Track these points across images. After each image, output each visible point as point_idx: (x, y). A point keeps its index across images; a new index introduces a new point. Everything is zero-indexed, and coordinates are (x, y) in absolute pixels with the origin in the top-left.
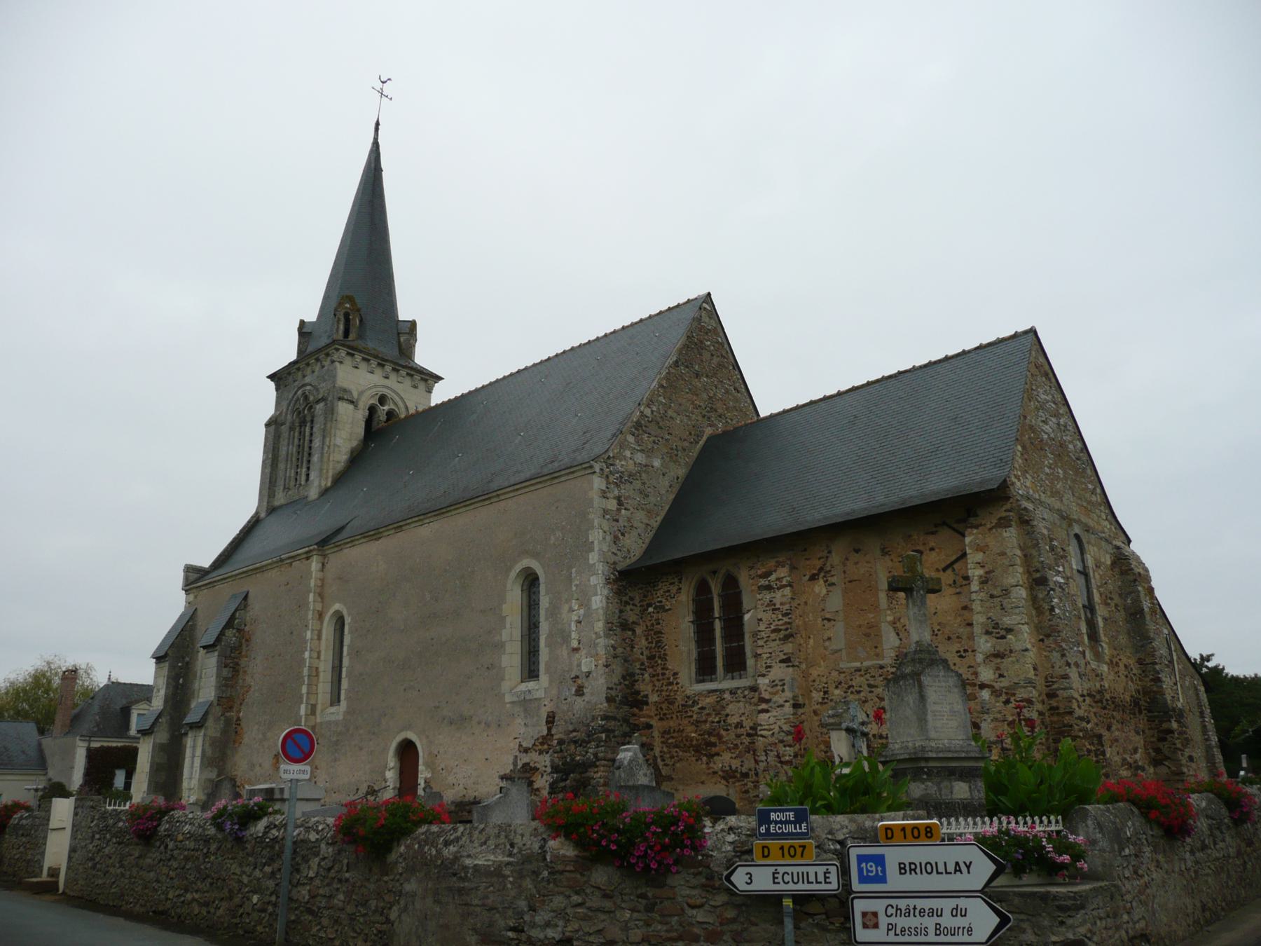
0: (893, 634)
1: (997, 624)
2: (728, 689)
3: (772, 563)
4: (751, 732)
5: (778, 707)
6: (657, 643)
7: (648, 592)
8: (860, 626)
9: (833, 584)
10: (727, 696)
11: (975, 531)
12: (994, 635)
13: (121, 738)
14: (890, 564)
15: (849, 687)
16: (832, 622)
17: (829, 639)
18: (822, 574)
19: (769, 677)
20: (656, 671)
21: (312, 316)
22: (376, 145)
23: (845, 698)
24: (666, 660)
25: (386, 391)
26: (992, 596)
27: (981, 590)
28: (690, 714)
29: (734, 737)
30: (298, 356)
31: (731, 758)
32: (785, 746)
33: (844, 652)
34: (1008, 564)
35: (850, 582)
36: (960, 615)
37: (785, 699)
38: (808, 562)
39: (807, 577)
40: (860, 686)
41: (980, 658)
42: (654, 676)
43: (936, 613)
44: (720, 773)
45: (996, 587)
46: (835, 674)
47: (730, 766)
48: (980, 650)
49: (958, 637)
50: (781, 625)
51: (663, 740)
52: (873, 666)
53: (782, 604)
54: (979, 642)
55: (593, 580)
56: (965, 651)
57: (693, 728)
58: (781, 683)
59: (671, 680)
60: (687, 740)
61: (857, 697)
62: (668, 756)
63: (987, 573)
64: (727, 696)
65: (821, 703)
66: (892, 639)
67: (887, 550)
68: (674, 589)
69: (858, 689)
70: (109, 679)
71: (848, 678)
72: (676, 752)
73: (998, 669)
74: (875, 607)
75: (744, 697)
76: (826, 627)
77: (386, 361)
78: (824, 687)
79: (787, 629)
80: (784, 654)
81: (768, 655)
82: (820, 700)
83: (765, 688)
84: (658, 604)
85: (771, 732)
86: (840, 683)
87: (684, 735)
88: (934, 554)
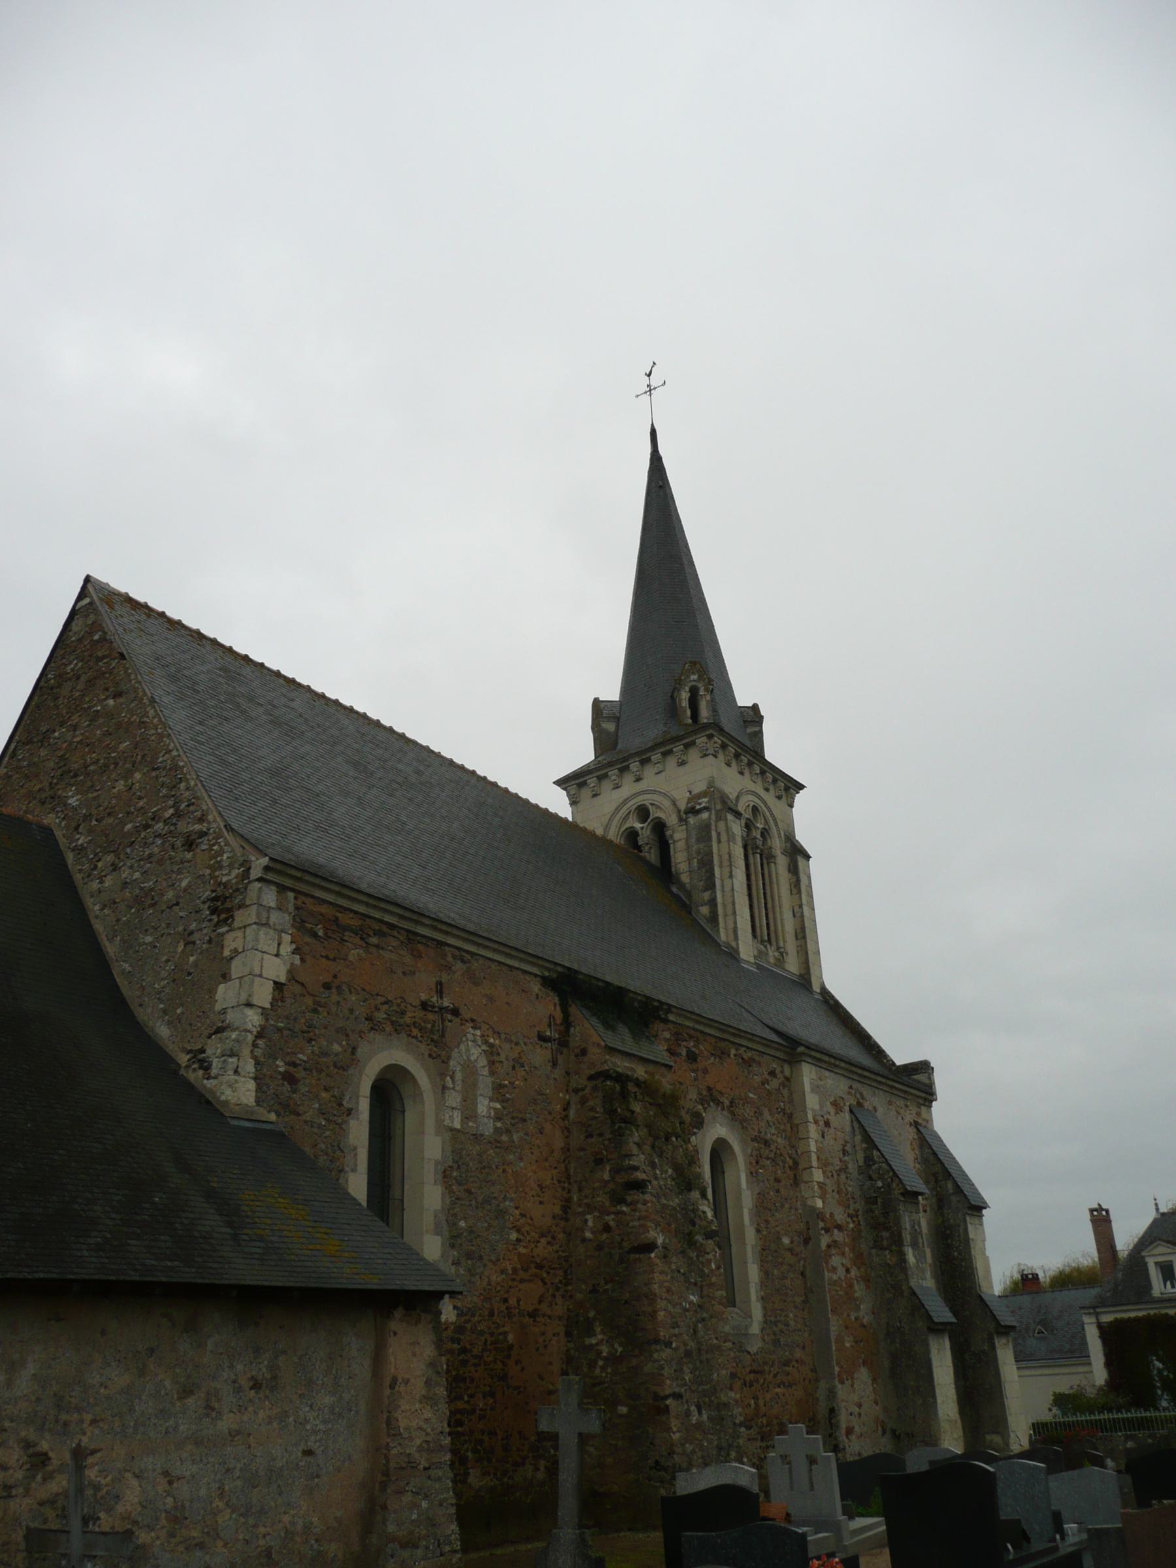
13: (1137, 1303)
21: (612, 692)
22: (656, 463)
25: (639, 800)
30: (597, 754)
70: (1157, 1209)
77: (625, 759)
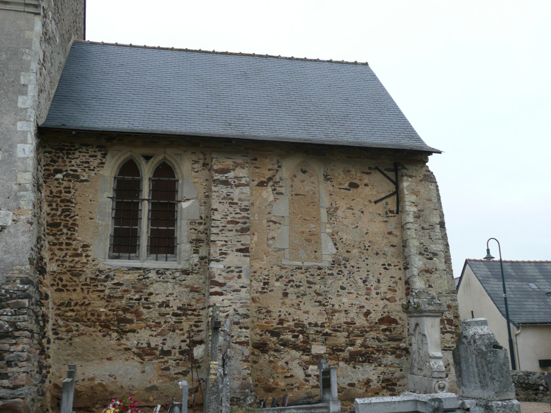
0: (331, 244)
1: (427, 248)
2: (154, 269)
3: (229, 163)
4: (179, 312)
5: (234, 291)
6: (63, 211)
7: (59, 157)
8: (303, 233)
9: (281, 194)
10: (153, 275)
11: (410, 179)
12: (425, 256)
14: (331, 188)
15: (290, 281)
16: (278, 225)
17: (273, 238)
18: (271, 183)
19: (223, 263)
20: (58, 239)
23: (286, 290)
24: (74, 230)
26: (423, 228)
27: (415, 222)
28: (100, 288)
29: (157, 315)
31: (152, 335)
32: (241, 328)
33: (287, 251)
34: (433, 207)
35: (296, 195)
36: (386, 238)
37: (241, 285)
38: (257, 170)
39: (256, 183)
40: (300, 282)
41: (415, 272)
42: (55, 244)
43: (367, 233)
44: (136, 350)
45: (425, 222)
46: (276, 268)
47: (149, 344)
48: (416, 266)
49: (384, 254)
50: (239, 218)
51: (58, 312)
52: (313, 267)
53: (240, 200)
54: (415, 260)
55: (21, 126)
56: (389, 265)
57: (104, 303)
58: (238, 270)
59: (79, 252)
60: (93, 315)
61: (297, 290)
62: (64, 329)
63: (419, 211)
64: (153, 275)
65: (261, 292)
66: (330, 247)
67: (328, 177)
68: (94, 163)
69: (298, 284)
71: (290, 274)
72: (77, 326)
73: (428, 281)
74: (317, 219)
75: (174, 278)
76: (271, 228)
78: (265, 279)
79: (245, 223)
80: (242, 244)
81: (224, 243)
82: (260, 290)
83: (219, 272)
84: (71, 173)
85: (225, 314)
86: (281, 277)
87: (89, 309)
88: (367, 189)
